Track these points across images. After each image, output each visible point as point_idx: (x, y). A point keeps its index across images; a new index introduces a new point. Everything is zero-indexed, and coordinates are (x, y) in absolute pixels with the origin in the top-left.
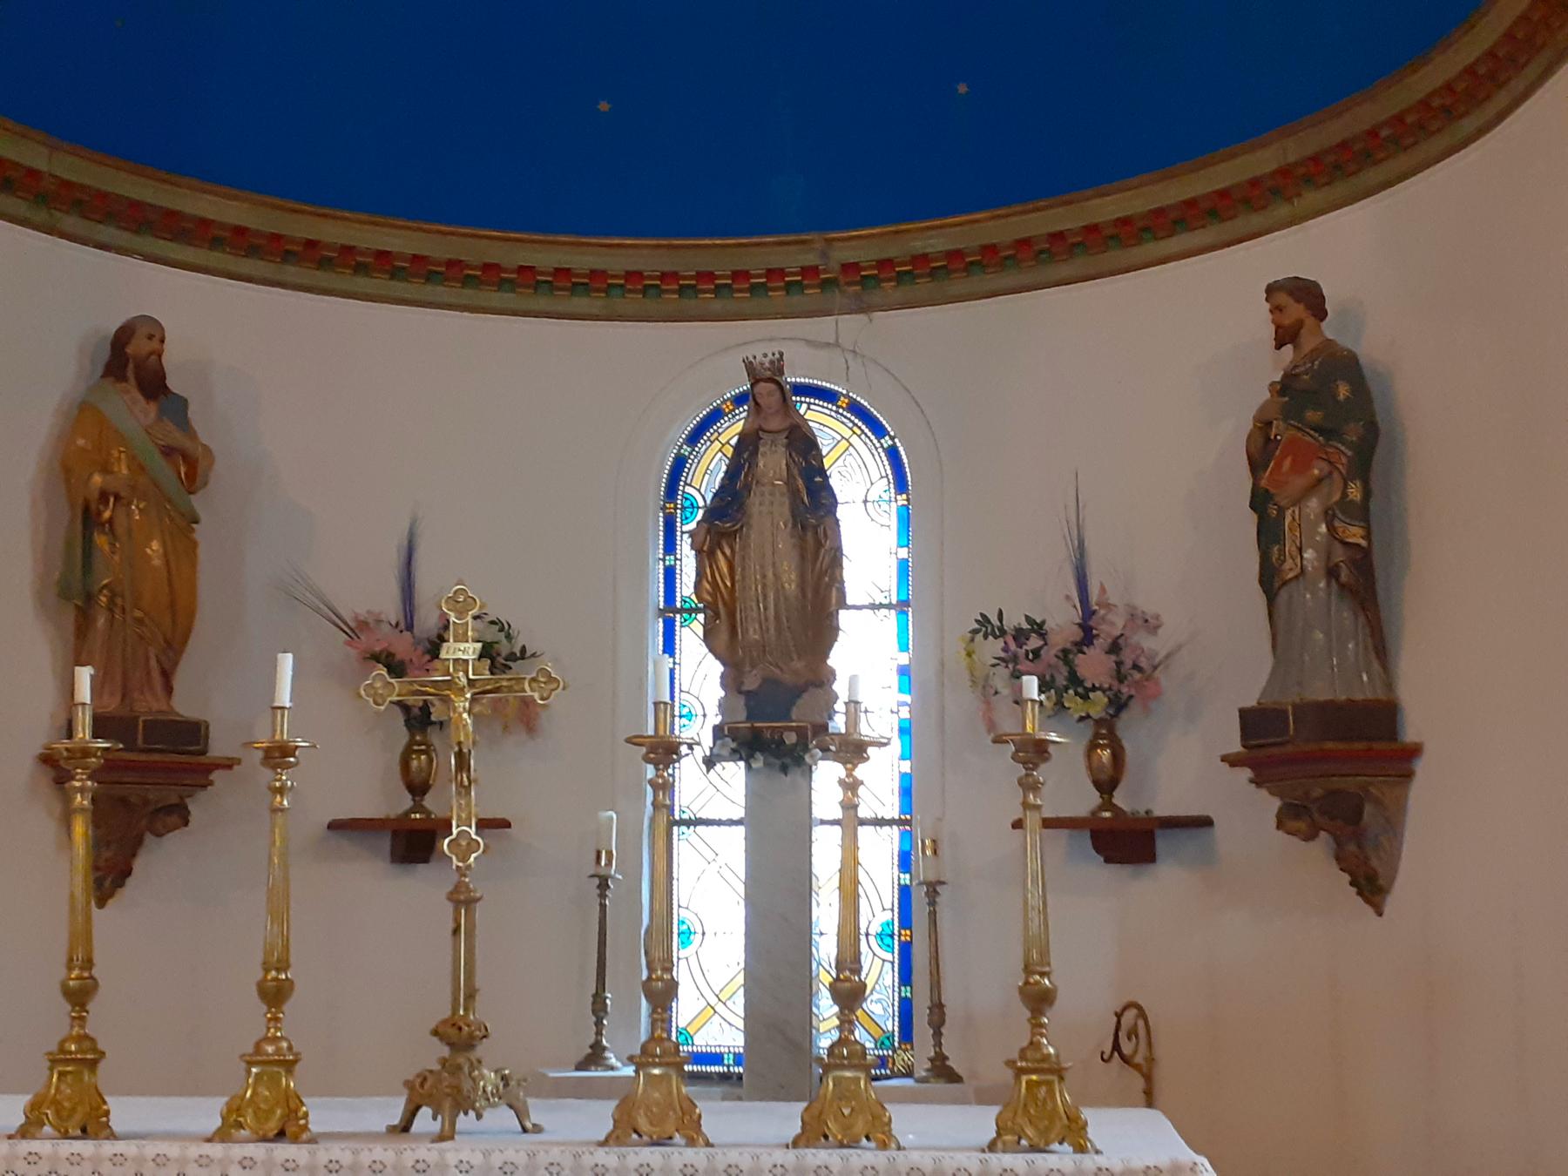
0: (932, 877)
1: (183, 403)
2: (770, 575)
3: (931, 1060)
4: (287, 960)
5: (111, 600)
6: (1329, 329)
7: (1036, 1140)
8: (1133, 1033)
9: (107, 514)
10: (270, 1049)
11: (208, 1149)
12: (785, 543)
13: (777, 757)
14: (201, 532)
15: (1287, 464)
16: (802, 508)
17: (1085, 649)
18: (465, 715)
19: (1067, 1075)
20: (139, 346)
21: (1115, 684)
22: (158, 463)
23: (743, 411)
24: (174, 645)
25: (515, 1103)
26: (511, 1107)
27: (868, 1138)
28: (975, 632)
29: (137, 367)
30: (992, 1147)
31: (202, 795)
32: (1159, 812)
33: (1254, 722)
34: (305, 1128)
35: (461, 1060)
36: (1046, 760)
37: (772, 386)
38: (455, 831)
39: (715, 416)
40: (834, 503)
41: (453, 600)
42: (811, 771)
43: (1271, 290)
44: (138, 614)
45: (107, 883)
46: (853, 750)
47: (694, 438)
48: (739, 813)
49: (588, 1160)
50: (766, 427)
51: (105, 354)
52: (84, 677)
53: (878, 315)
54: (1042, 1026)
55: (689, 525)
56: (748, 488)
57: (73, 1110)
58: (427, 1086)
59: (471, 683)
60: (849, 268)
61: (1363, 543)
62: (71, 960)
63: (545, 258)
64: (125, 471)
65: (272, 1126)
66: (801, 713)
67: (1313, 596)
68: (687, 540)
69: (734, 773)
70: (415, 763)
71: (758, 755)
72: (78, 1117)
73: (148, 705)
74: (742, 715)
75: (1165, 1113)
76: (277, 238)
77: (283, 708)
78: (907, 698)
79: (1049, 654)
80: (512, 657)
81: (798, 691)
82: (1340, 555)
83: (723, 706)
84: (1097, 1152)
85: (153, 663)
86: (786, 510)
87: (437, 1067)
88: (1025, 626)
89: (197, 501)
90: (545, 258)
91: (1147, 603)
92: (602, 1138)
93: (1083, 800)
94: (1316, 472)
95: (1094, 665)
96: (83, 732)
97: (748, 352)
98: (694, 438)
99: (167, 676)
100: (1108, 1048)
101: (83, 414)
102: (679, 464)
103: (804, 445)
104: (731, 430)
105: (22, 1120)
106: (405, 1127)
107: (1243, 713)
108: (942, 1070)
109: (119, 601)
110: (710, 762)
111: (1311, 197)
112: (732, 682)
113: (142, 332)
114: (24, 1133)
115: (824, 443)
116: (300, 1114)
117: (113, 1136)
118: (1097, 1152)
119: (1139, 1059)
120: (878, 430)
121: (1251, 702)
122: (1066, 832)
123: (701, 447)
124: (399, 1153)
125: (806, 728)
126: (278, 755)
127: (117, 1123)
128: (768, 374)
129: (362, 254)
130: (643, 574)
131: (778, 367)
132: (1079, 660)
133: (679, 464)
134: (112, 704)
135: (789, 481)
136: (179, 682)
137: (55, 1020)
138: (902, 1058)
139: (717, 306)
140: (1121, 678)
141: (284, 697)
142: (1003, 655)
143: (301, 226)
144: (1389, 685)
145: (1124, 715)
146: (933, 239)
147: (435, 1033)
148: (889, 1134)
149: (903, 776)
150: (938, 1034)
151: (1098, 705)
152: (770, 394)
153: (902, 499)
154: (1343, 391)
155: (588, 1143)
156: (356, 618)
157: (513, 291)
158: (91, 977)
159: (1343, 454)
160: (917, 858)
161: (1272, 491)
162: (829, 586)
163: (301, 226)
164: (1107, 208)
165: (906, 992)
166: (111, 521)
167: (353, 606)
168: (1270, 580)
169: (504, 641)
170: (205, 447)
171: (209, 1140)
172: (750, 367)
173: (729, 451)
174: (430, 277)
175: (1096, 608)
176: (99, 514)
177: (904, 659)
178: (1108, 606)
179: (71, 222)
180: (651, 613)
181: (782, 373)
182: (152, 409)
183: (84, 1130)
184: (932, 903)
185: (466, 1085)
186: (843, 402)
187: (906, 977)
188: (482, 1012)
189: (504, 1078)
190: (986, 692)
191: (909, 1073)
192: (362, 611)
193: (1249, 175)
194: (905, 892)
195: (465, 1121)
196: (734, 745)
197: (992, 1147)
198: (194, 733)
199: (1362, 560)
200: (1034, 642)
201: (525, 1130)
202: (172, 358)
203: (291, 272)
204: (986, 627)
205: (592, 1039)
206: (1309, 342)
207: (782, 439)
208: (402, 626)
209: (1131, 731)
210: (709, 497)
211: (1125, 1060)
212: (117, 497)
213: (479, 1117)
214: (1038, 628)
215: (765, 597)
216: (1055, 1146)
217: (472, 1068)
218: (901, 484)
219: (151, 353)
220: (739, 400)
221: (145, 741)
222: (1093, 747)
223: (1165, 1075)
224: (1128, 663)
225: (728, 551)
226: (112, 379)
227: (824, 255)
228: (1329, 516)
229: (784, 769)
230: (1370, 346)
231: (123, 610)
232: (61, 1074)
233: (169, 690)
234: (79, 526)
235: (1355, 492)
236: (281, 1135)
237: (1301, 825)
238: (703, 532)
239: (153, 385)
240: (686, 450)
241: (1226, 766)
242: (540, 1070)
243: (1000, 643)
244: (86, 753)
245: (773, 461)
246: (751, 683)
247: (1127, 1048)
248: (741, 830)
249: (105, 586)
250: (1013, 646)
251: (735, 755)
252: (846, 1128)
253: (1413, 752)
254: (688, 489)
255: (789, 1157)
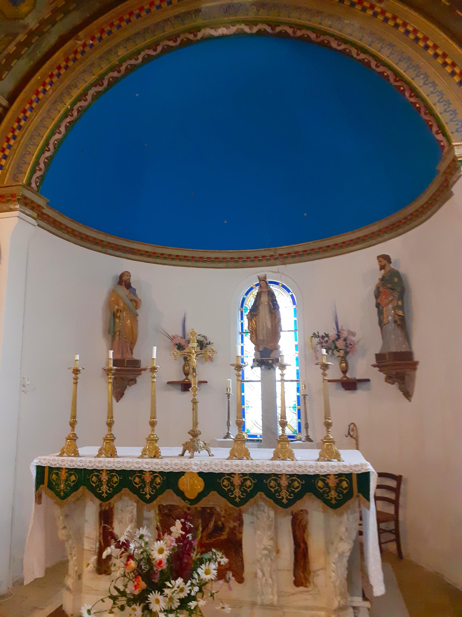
0: (304, 394)
1: (135, 290)
2: (265, 324)
3: (306, 437)
4: (156, 416)
5: (119, 334)
6: (392, 266)
7: (329, 458)
8: (353, 430)
9: (118, 315)
10: (152, 437)
11: (138, 460)
12: (268, 317)
13: (268, 366)
14: (138, 318)
15: (384, 297)
16: (271, 309)
17: (338, 340)
18: (194, 360)
19: (336, 443)
20: (125, 278)
21: (346, 348)
22: (128, 302)
23: (258, 287)
24: (133, 343)
25: (207, 449)
26: (207, 450)
27: (289, 458)
28: (312, 337)
29: (125, 282)
30: (318, 460)
31: (140, 376)
32: (358, 377)
33: (379, 357)
34: (160, 455)
35: (195, 439)
36: (328, 369)
37: (264, 282)
38: (192, 386)
39: (252, 289)
40: (278, 308)
41: (191, 333)
42: (275, 369)
43: (379, 257)
44: (125, 336)
45: (119, 397)
46: (283, 367)
47: (247, 294)
48: (259, 379)
49: (224, 463)
50: (263, 291)
51: (118, 280)
52: (111, 352)
53: (288, 265)
54: (329, 431)
55: (246, 313)
56: (259, 305)
57: (109, 451)
58: (187, 445)
59: (196, 352)
60: (281, 255)
61: (402, 315)
62: (108, 417)
63: (213, 255)
64: (122, 305)
65: (153, 456)
66: (273, 356)
67: (391, 327)
68: (246, 316)
69: (258, 370)
70: (186, 369)
71: (263, 366)
72: (110, 453)
73: (128, 357)
74: (259, 356)
75: (361, 452)
76: (154, 253)
77: (154, 359)
78: (298, 352)
79: (330, 342)
80: (207, 344)
81: (272, 351)
82: (397, 318)
83: (255, 355)
84: (343, 461)
85: (128, 347)
86: (268, 309)
87: (190, 441)
88: (324, 335)
89: (138, 311)
90: (213, 255)
91: (352, 330)
92: (227, 458)
93: (339, 375)
94: (390, 299)
95: (340, 344)
96: (111, 365)
97: (258, 274)
98: (247, 294)
99: (131, 350)
100: (347, 433)
101: (113, 293)
102: (244, 299)
103: (271, 295)
104: (255, 292)
105: (98, 453)
106: (183, 455)
107: (377, 355)
108: (308, 439)
109: (121, 334)
110: (252, 367)
111: (386, 236)
112: (257, 349)
113: (126, 274)
114: (98, 456)
115: (276, 294)
116: (159, 452)
117: (118, 457)
118: (343, 461)
119: (354, 436)
120: (289, 291)
121: (378, 352)
122: (335, 383)
123: (248, 296)
124: (181, 461)
125: (274, 359)
126: (153, 369)
127: (118, 454)
128: (263, 279)
129: (173, 256)
130: (236, 323)
131: (265, 278)
132: (337, 343)
133: (244, 300)
134: (119, 357)
135: (268, 303)
136: (134, 351)
137: (105, 431)
138: (299, 436)
139: (252, 264)
140: (347, 346)
141: (154, 356)
142: (319, 342)
143: (160, 250)
144: (410, 347)
145: (348, 355)
146: (299, 248)
147: (189, 433)
148: (294, 457)
149: (297, 370)
150: (307, 431)
151: (342, 353)
152: (264, 283)
153: (295, 306)
154: (396, 280)
155: (224, 459)
156: (173, 336)
157: (206, 262)
158: (113, 420)
159: (396, 295)
160: (301, 389)
161: (380, 303)
162: (278, 326)
163: (160, 250)
164: (339, 240)
165: (299, 421)
166: (119, 316)
167: (171, 334)
168: (381, 323)
169: (205, 340)
170: (140, 300)
171: (139, 458)
172: (259, 278)
173: (255, 297)
174: (188, 260)
175: (340, 331)
176: (117, 315)
177: (297, 343)
178: (342, 330)
179: (110, 251)
180: (238, 333)
181: (266, 279)
182: (128, 291)
183: (111, 455)
184: (305, 400)
185: (196, 445)
186: (280, 285)
187: (299, 417)
188: (199, 428)
189: (205, 444)
190: (316, 351)
191: (300, 440)
192: (174, 334)
193: (371, 232)
194: (298, 397)
195: (196, 453)
196: (257, 363)
197: (318, 460)
198: (136, 363)
199: (403, 319)
200: (326, 339)
201: (210, 456)
202: (132, 280)
203: (158, 260)
204: (315, 335)
205: (227, 432)
206: (387, 269)
207: (266, 293)
208: (183, 337)
209: (350, 358)
210: (251, 307)
211: (351, 436)
212: (121, 311)
213: (199, 452)
214: (327, 336)
215: (264, 329)
216: (333, 460)
217: (198, 441)
218: (294, 303)
219: (128, 279)
220: (257, 285)
221: (127, 364)
222: (341, 363)
223: (360, 439)
224: (348, 344)
225: (255, 319)
226: (119, 285)
227: (275, 252)
228: (394, 309)
229: (269, 369)
230: (402, 270)
231: (122, 336)
232: (106, 443)
233: (132, 353)
234: (112, 317)
235: (400, 303)
236: (155, 457)
237: (391, 381)
238: (249, 315)
239: (128, 286)
240: (245, 297)
241: (372, 367)
242: (215, 439)
243: (318, 339)
244: (111, 370)
245: (265, 299)
246: (261, 349)
247: (352, 433)
248: (260, 383)
249: (118, 331)
250: (321, 340)
251: (258, 366)
252: (284, 456)
253: (416, 363)
254: (246, 305)
255: (270, 462)
